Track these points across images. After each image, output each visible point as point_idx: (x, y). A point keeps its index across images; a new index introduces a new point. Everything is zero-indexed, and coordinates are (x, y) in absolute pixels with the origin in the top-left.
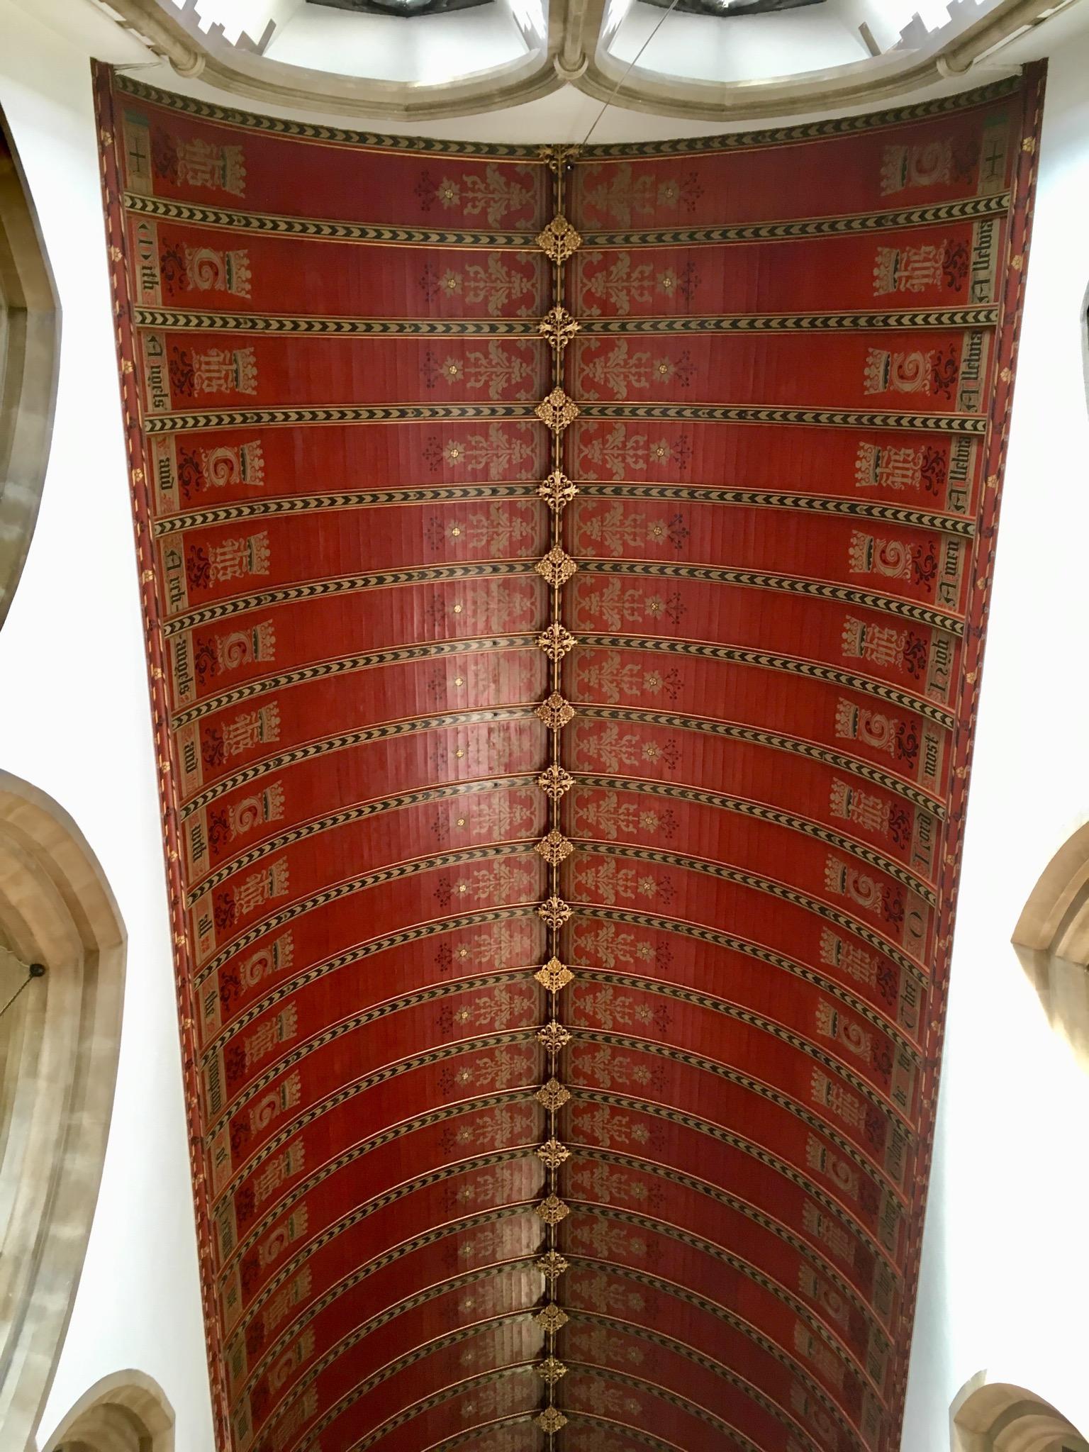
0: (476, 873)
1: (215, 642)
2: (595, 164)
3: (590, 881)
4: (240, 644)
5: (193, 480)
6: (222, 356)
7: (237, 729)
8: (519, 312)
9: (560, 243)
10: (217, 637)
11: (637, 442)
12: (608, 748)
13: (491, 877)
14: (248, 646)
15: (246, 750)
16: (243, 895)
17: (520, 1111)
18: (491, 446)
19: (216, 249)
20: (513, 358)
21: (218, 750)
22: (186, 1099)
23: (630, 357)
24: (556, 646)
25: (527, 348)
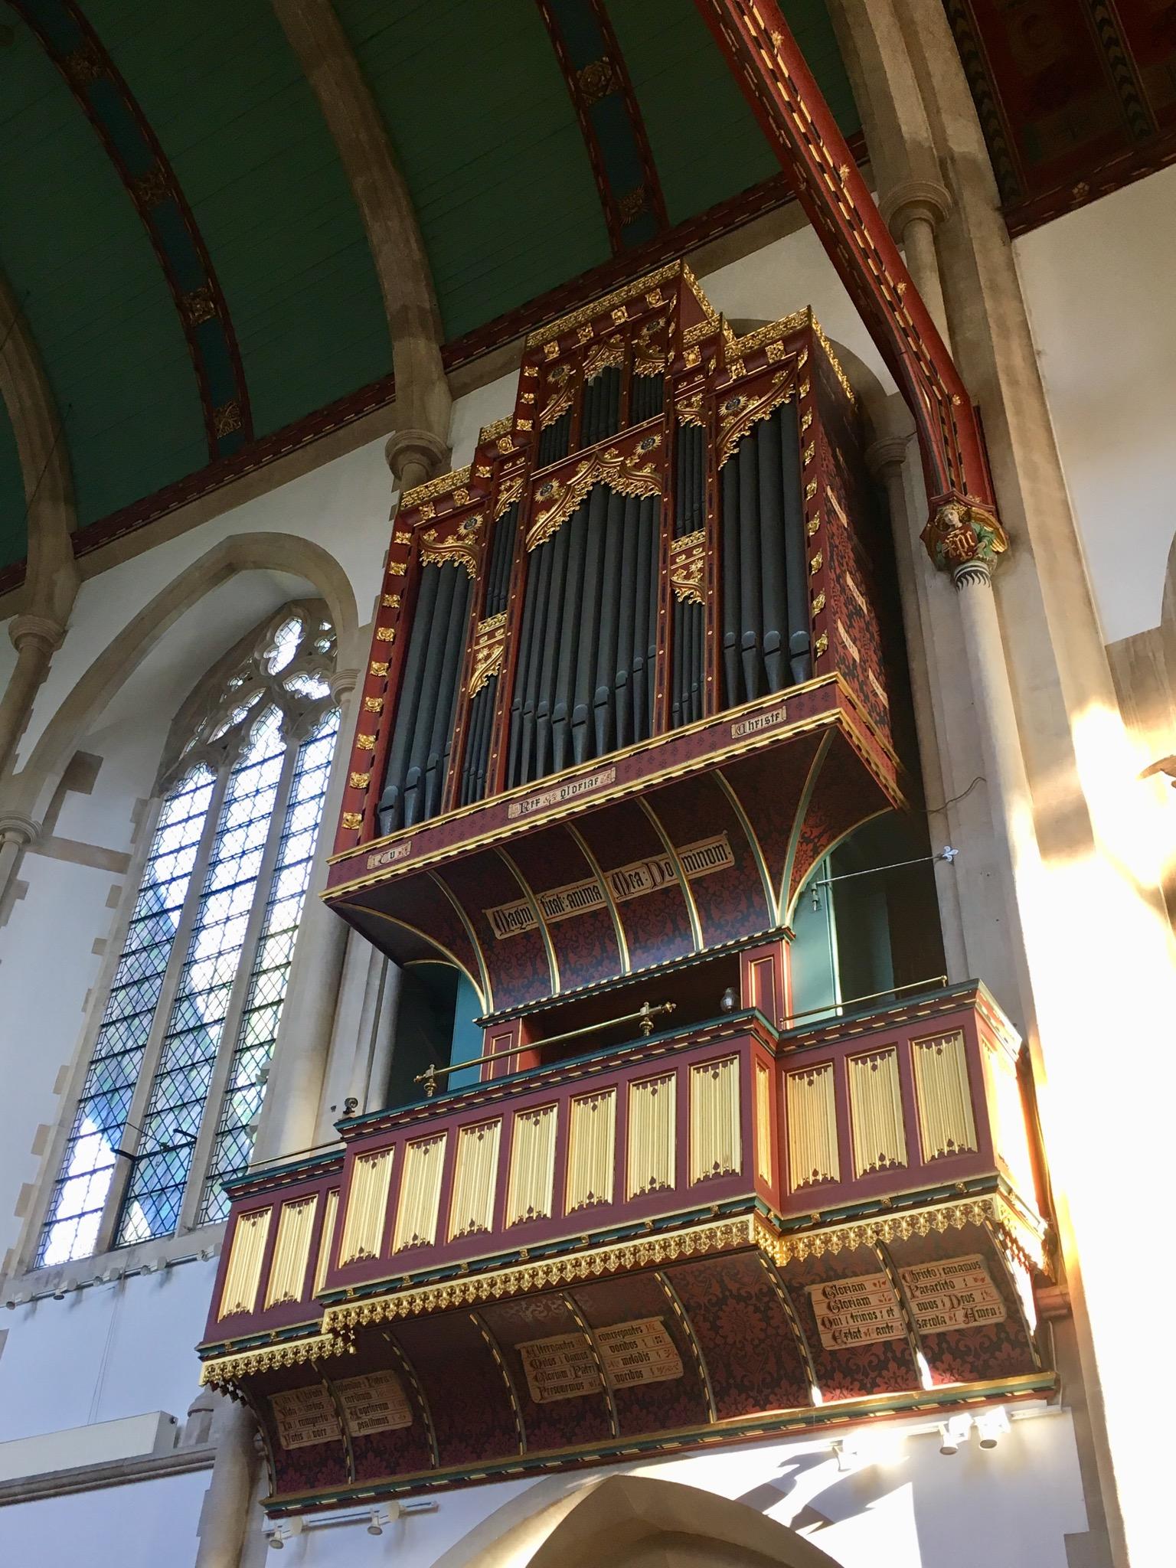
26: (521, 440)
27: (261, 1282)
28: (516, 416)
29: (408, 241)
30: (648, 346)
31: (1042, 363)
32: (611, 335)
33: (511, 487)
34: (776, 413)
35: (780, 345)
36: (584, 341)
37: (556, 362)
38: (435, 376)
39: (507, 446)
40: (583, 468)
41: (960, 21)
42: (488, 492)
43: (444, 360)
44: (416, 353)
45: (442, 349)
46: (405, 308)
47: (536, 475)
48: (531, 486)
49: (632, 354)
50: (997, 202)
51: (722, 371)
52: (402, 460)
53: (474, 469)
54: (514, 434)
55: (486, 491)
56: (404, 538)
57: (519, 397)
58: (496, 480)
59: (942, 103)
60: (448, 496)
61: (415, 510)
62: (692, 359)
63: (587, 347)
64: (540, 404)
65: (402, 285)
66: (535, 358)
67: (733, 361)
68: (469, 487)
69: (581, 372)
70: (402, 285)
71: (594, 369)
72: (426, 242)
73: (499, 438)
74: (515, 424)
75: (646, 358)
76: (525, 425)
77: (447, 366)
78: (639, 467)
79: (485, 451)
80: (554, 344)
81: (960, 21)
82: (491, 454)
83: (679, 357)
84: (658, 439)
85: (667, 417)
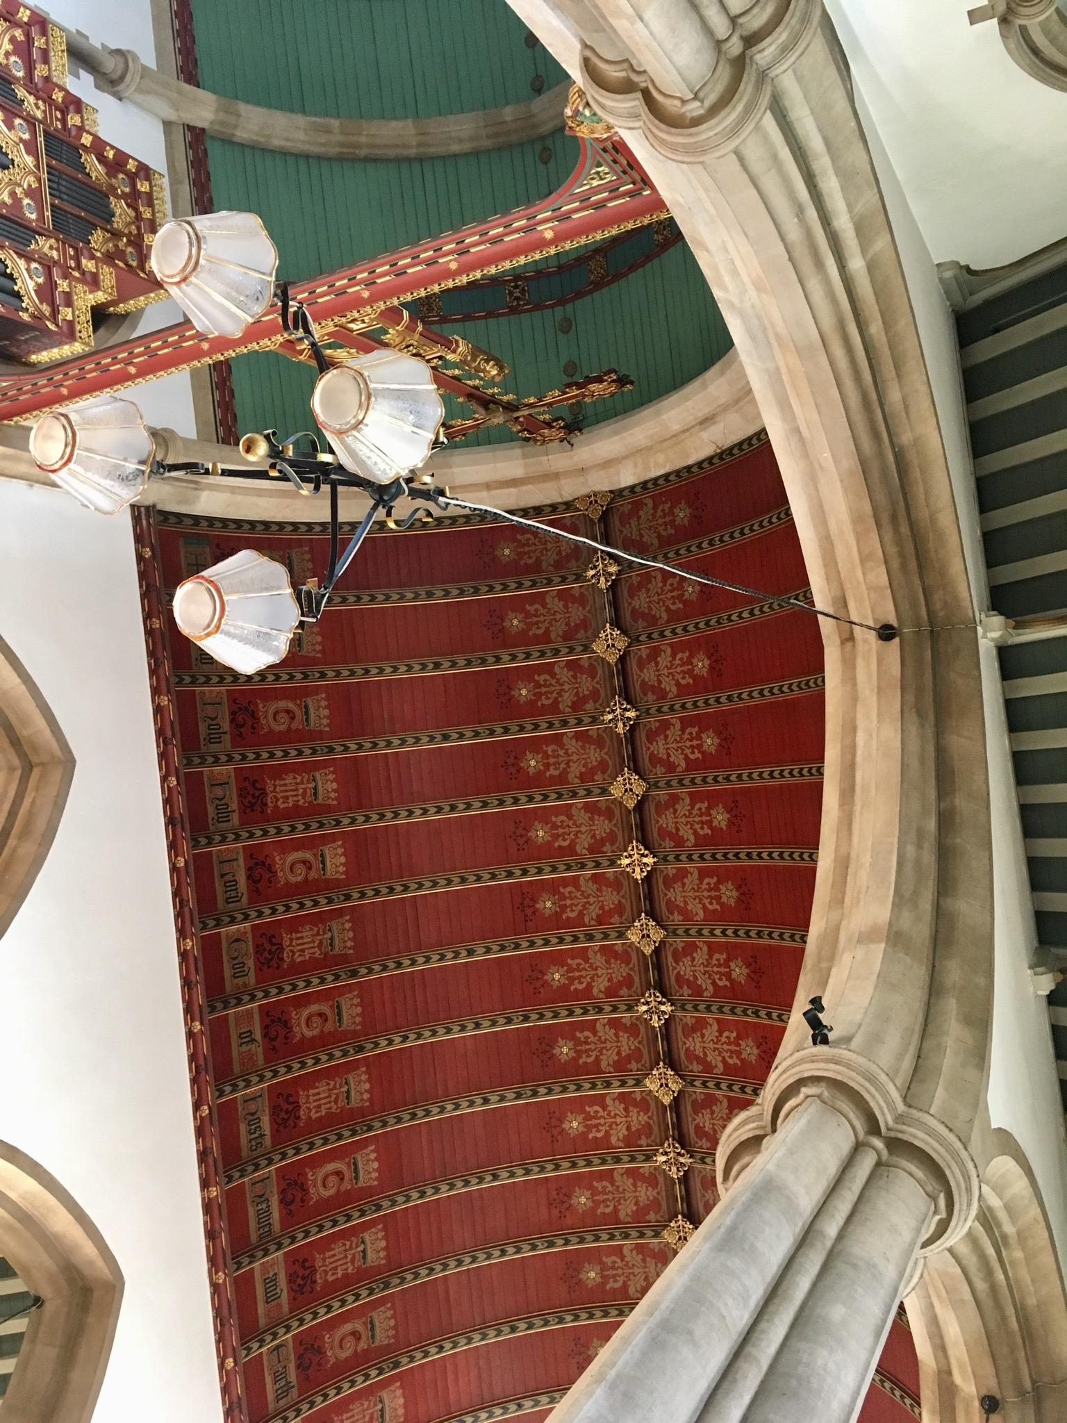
0: (554, 819)
1: (257, 705)
2: (625, 506)
3: (661, 750)
4: (321, 1015)
5: (298, 1199)
6: (316, 929)
7: (302, 938)
8: (605, 849)
9: (664, 1081)
10: (307, 1170)
11: (691, 734)
12: (674, 745)
13: (561, 753)
14: (313, 863)
15: (346, 1276)
16: (328, 1261)
17: (643, 1178)
18: (609, 1114)
19: (293, 699)
20: (639, 1184)
21: (310, 1278)
22: (137, 550)
23: (683, 733)
24: (636, 857)
25: (632, 1024)
26: (74, 132)
27: (1038, 259)
28: (96, 138)
29: (287, 140)
30: (116, 246)
31: (22, 484)
32: (139, 228)
33: (38, 108)
34: (18, 296)
35: (70, 317)
36: (142, 209)
37: (134, 186)
38: (182, 114)
39: (74, 120)
40: (29, 160)
41: (291, 528)
42: (42, 91)
43: (195, 128)
44: (203, 109)
45: (203, 130)
46: (239, 116)
47: (40, 130)
48: (31, 122)
49: (116, 235)
50: (159, 507)
51: (65, 276)
52: (120, 60)
53: (62, 89)
54: (81, 129)
55: (42, 91)
56: (24, 15)
57: (113, 147)
58: (49, 101)
59: (239, 498)
60: (46, 61)
61: (44, 33)
62: (89, 265)
63: (136, 210)
64: (102, 159)
65: (257, 123)
66: (142, 174)
67: (70, 285)
68: (47, 79)
69: (118, 197)
70: (257, 123)
71: (120, 209)
72: (284, 154)
73: (82, 117)
74: (88, 132)
75: (106, 241)
76: (86, 140)
77: (191, 128)
78: (13, 194)
79: (75, 104)
80: (148, 190)
81: (291, 528)
82: (72, 108)
83: (92, 257)
84: (33, 216)
85: (47, 230)
